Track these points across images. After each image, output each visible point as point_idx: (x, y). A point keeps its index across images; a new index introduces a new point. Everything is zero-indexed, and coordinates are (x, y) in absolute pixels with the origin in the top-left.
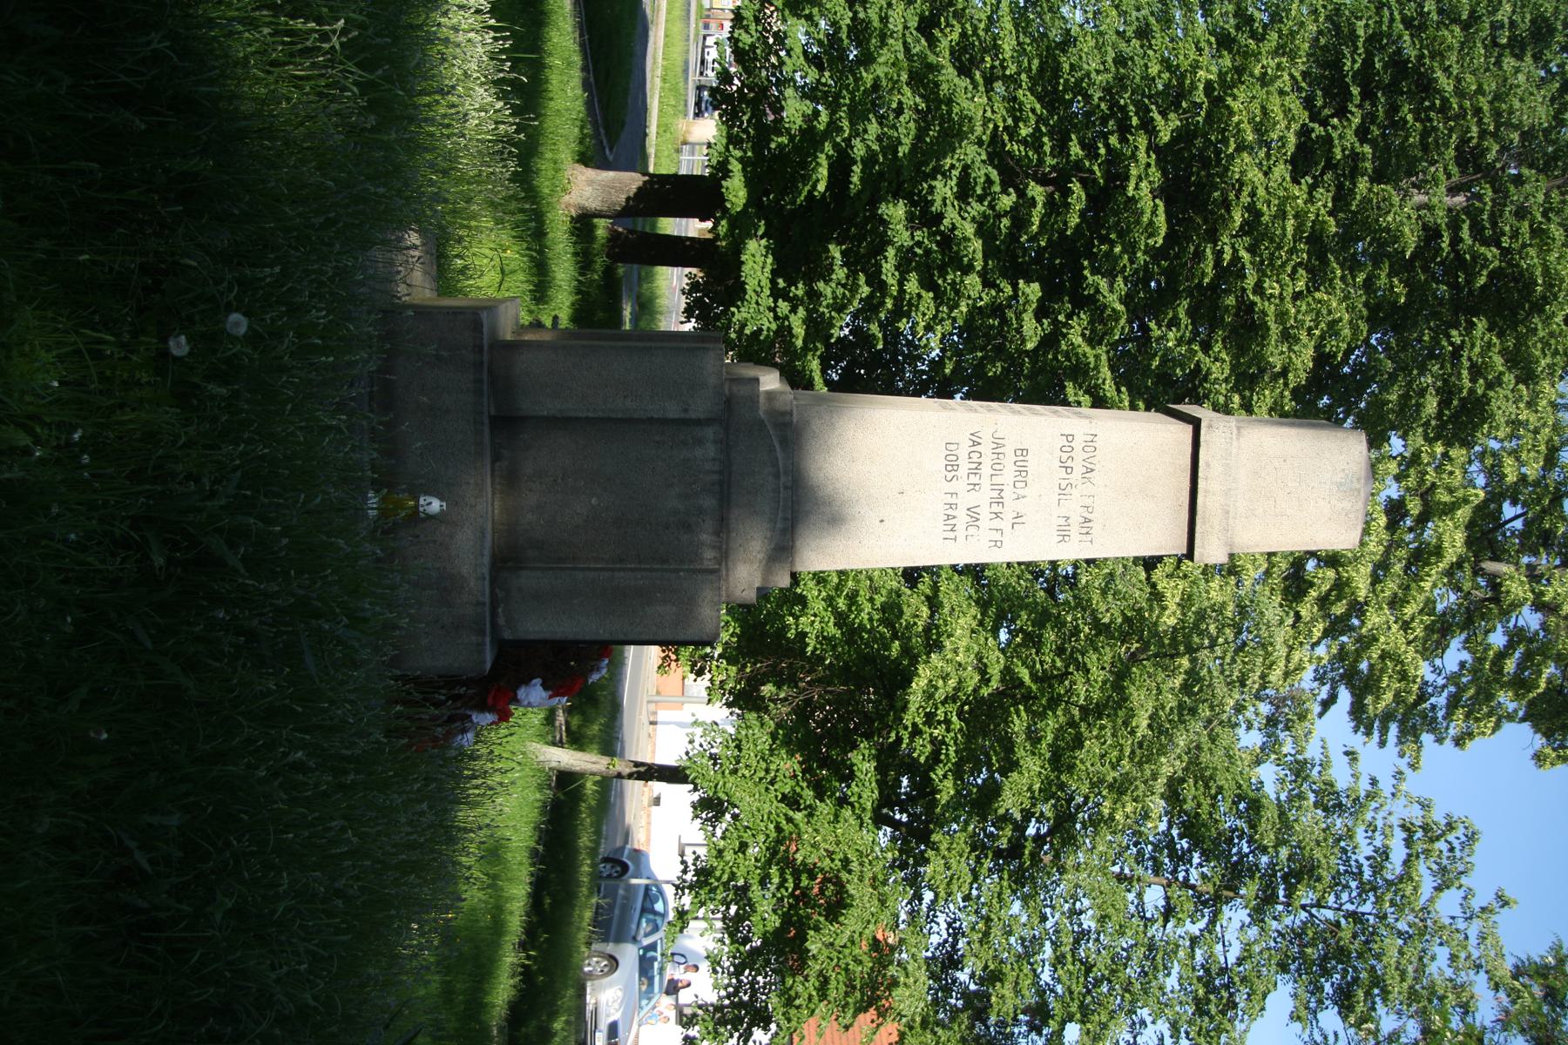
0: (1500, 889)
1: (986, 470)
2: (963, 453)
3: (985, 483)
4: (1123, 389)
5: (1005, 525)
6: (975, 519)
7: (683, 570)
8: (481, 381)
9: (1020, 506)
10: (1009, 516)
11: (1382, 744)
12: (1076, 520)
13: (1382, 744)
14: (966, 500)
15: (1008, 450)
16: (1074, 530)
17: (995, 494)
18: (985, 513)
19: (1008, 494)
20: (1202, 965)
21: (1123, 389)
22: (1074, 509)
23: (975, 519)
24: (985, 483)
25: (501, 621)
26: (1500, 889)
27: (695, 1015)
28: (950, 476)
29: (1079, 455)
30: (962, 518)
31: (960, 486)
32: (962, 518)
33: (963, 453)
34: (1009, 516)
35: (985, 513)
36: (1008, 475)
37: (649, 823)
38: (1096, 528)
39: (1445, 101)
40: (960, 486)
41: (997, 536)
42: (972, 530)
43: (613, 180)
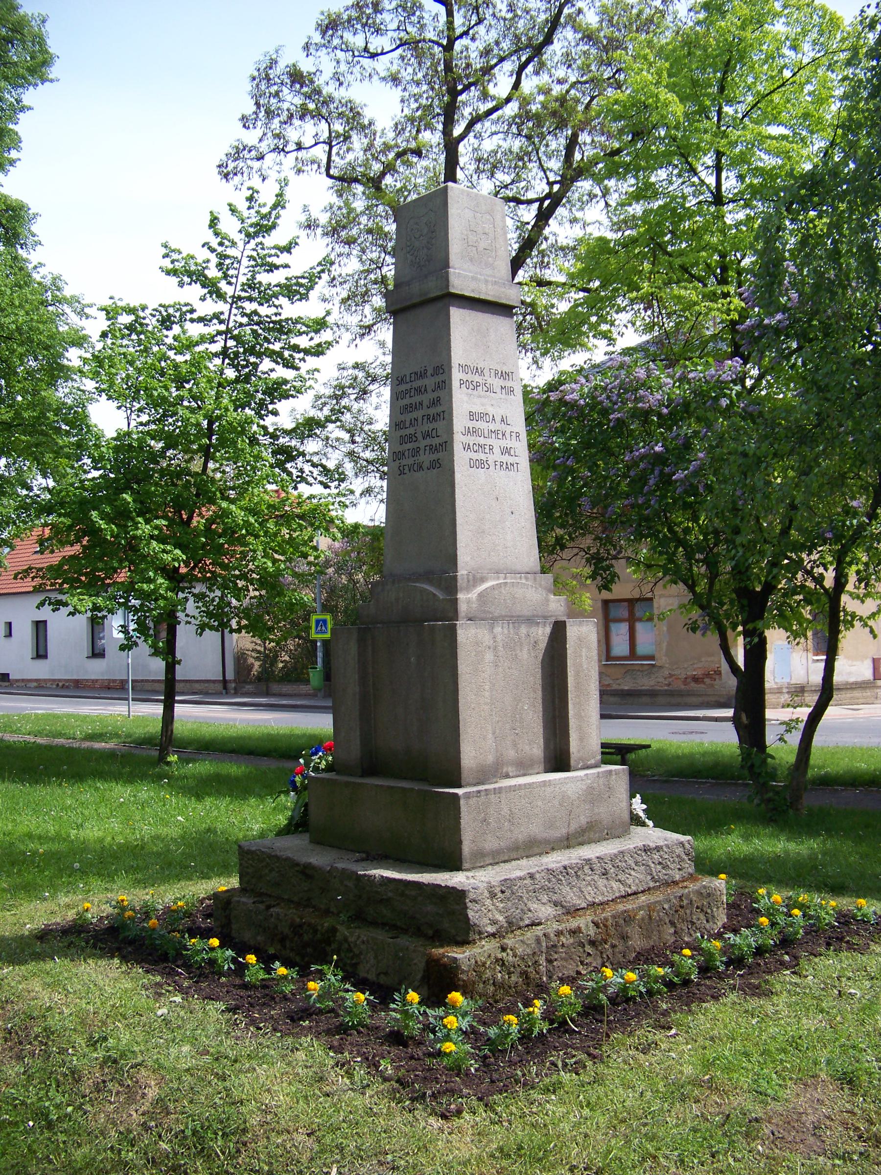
1: (482, 441)
2: (475, 456)
3: (489, 442)
5: (508, 429)
7: (705, 985)
8: (479, 792)
10: (503, 427)
12: (502, 382)
14: (497, 456)
15: (471, 424)
16: (509, 384)
19: (492, 426)
20: (747, 205)
22: (497, 383)
24: (489, 442)
27: (633, 997)
29: (470, 377)
30: (506, 458)
31: (491, 458)
32: (506, 458)
34: (503, 427)
36: (481, 425)
37: (23, 680)
38: (505, 369)
41: (514, 435)
43: (275, 720)
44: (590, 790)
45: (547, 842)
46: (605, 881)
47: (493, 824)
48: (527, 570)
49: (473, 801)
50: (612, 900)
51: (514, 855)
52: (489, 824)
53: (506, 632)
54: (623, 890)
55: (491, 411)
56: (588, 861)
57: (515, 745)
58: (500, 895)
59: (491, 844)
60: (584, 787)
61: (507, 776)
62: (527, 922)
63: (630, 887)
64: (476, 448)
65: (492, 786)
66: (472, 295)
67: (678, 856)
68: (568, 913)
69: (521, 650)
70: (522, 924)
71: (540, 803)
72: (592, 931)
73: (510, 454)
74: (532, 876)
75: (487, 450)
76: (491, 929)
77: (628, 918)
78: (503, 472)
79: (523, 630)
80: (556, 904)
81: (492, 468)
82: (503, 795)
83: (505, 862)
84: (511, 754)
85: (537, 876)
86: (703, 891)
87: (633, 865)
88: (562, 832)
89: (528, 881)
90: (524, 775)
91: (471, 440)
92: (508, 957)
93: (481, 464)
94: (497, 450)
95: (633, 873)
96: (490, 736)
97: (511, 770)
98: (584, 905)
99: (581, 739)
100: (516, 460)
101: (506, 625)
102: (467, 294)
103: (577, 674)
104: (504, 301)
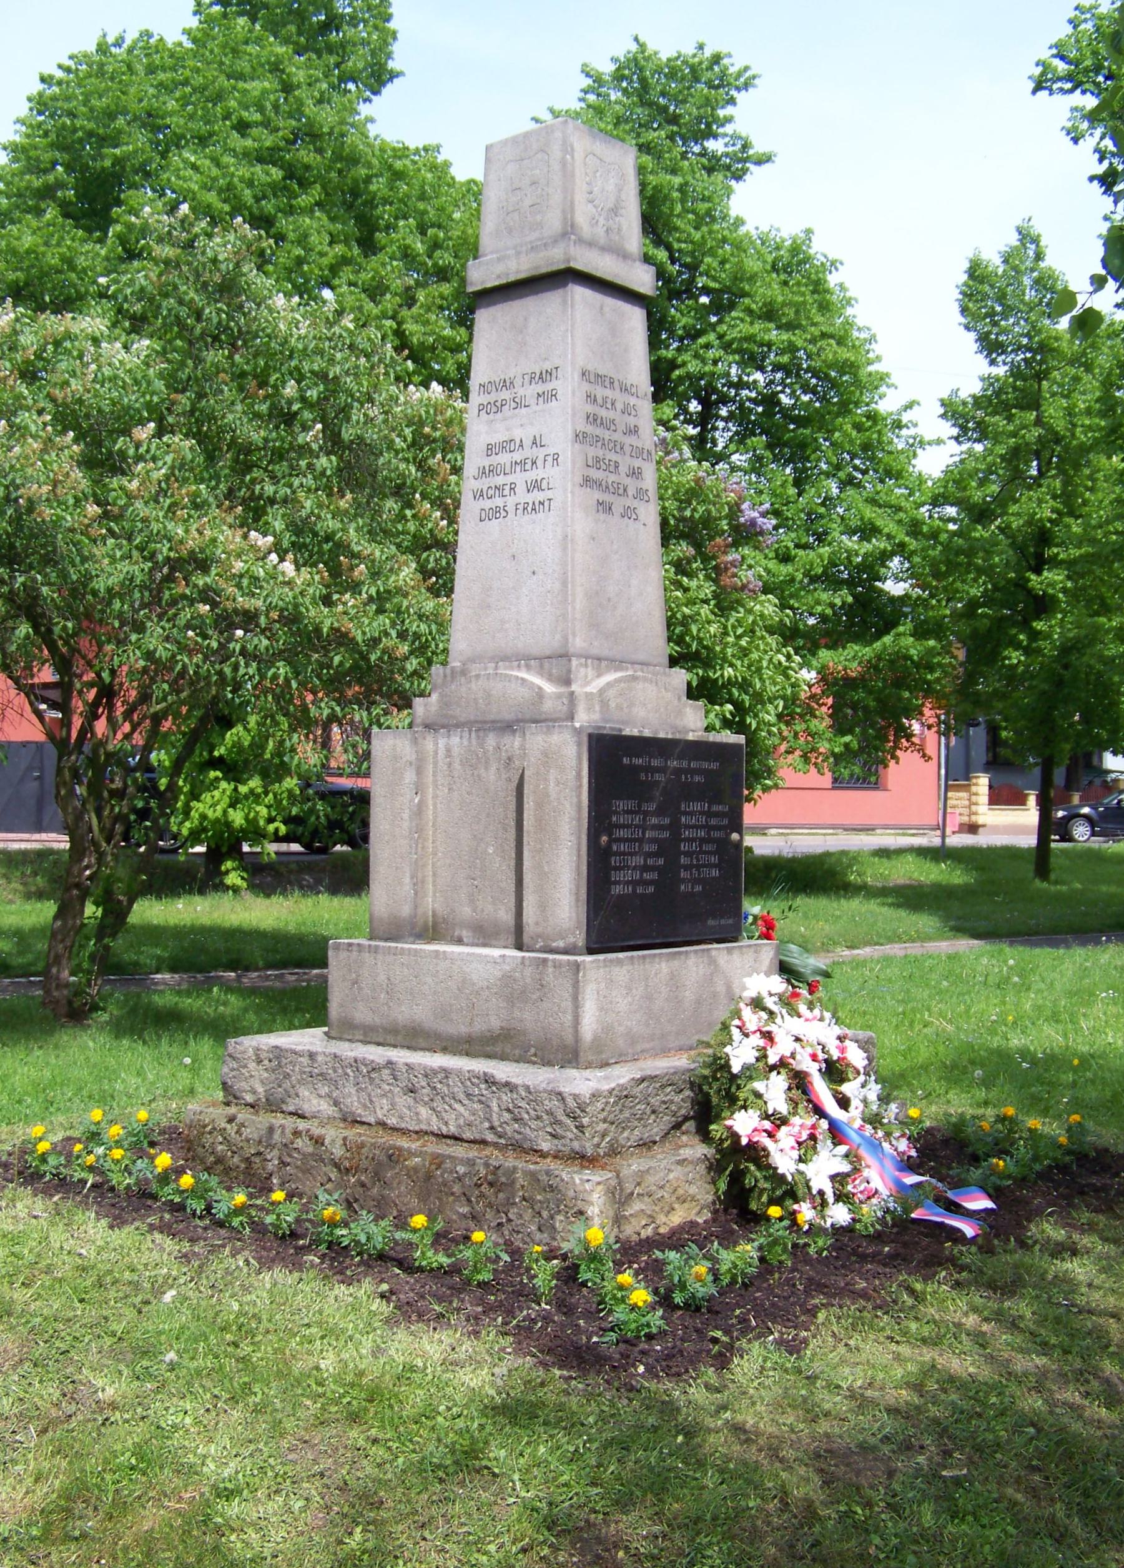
0: (585, 65)
1: (500, 480)
2: (488, 504)
4: (698, 888)
5: (541, 453)
6: (536, 485)
8: (350, 945)
9: (527, 443)
11: (60, 67)
12: (540, 388)
13: (60, 67)
14: (522, 496)
17: (518, 468)
18: (532, 475)
19: (517, 456)
21: (698, 888)
23: (536, 485)
24: (510, 479)
25: (561, 944)
26: (585, 65)
28: (503, 514)
30: (538, 496)
32: (538, 496)
33: (488, 504)
35: (532, 475)
36: (504, 458)
38: (548, 366)
39: (124, 382)
40: (511, 501)
41: (550, 459)
42: (544, 485)
44: (507, 979)
45: (438, 1036)
46: (411, 1101)
47: (367, 991)
48: (548, 653)
49: (343, 955)
50: (417, 1132)
51: (390, 1039)
52: (360, 989)
53: (466, 743)
54: (435, 1125)
55: (518, 434)
56: (390, 1063)
57: (472, 901)
58: (266, 1062)
59: (362, 1014)
60: (499, 974)
61: (460, 941)
62: (291, 1108)
63: (446, 1124)
64: (491, 492)
65: (406, 946)
66: (497, 283)
67: (550, 1113)
68: (345, 1120)
69: (486, 769)
70: (284, 1108)
71: (429, 980)
72: (338, 1152)
73: (540, 489)
74: (312, 1056)
75: (506, 492)
76: (249, 1098)
77: (394, 1157)
78: (527, 517)
79: (491, 740)
80: (336, 1103)
81: (511, 515)
82: (380, 957)
83: (379, 1044)
84: (466, 912)
85: (320, 1058)
86: (544, 1178)
87: (462, 1096)
88: (459, 1028)
89: (305, 1060)
90: (485, 945)
91: (484, 484)
92: (231, 1129)
93: (496, 513)
94: (623, 469)
95: (457, 1106)
96: (407, 880)
97: (465, 934)
98: (372, 1120)
99: (543, 907)
100: (549, 494)
101: (466, 734)
102: (489, 285)
103: (539, 805)
104: (544, 270)
